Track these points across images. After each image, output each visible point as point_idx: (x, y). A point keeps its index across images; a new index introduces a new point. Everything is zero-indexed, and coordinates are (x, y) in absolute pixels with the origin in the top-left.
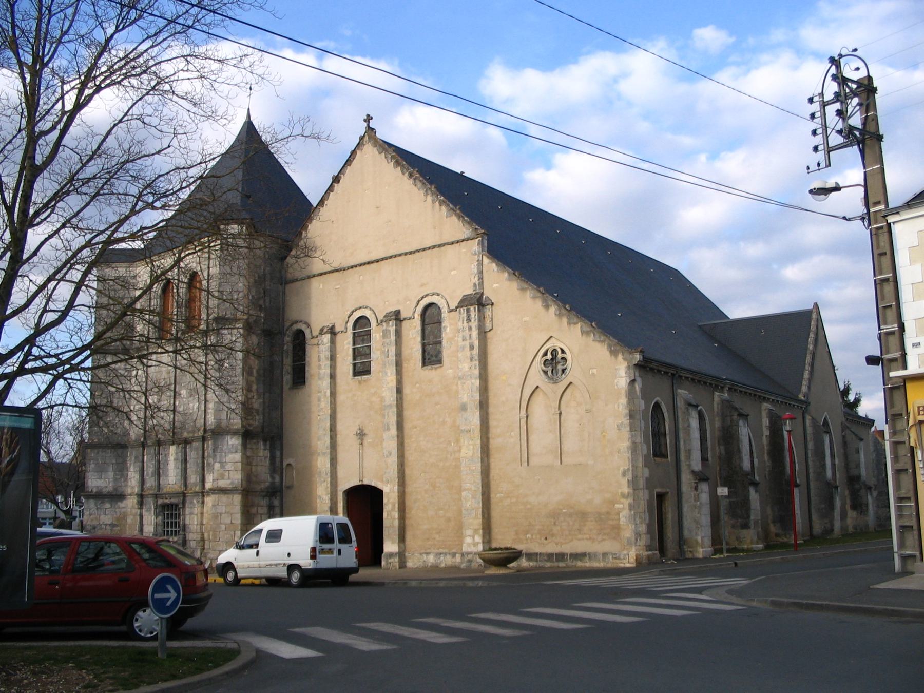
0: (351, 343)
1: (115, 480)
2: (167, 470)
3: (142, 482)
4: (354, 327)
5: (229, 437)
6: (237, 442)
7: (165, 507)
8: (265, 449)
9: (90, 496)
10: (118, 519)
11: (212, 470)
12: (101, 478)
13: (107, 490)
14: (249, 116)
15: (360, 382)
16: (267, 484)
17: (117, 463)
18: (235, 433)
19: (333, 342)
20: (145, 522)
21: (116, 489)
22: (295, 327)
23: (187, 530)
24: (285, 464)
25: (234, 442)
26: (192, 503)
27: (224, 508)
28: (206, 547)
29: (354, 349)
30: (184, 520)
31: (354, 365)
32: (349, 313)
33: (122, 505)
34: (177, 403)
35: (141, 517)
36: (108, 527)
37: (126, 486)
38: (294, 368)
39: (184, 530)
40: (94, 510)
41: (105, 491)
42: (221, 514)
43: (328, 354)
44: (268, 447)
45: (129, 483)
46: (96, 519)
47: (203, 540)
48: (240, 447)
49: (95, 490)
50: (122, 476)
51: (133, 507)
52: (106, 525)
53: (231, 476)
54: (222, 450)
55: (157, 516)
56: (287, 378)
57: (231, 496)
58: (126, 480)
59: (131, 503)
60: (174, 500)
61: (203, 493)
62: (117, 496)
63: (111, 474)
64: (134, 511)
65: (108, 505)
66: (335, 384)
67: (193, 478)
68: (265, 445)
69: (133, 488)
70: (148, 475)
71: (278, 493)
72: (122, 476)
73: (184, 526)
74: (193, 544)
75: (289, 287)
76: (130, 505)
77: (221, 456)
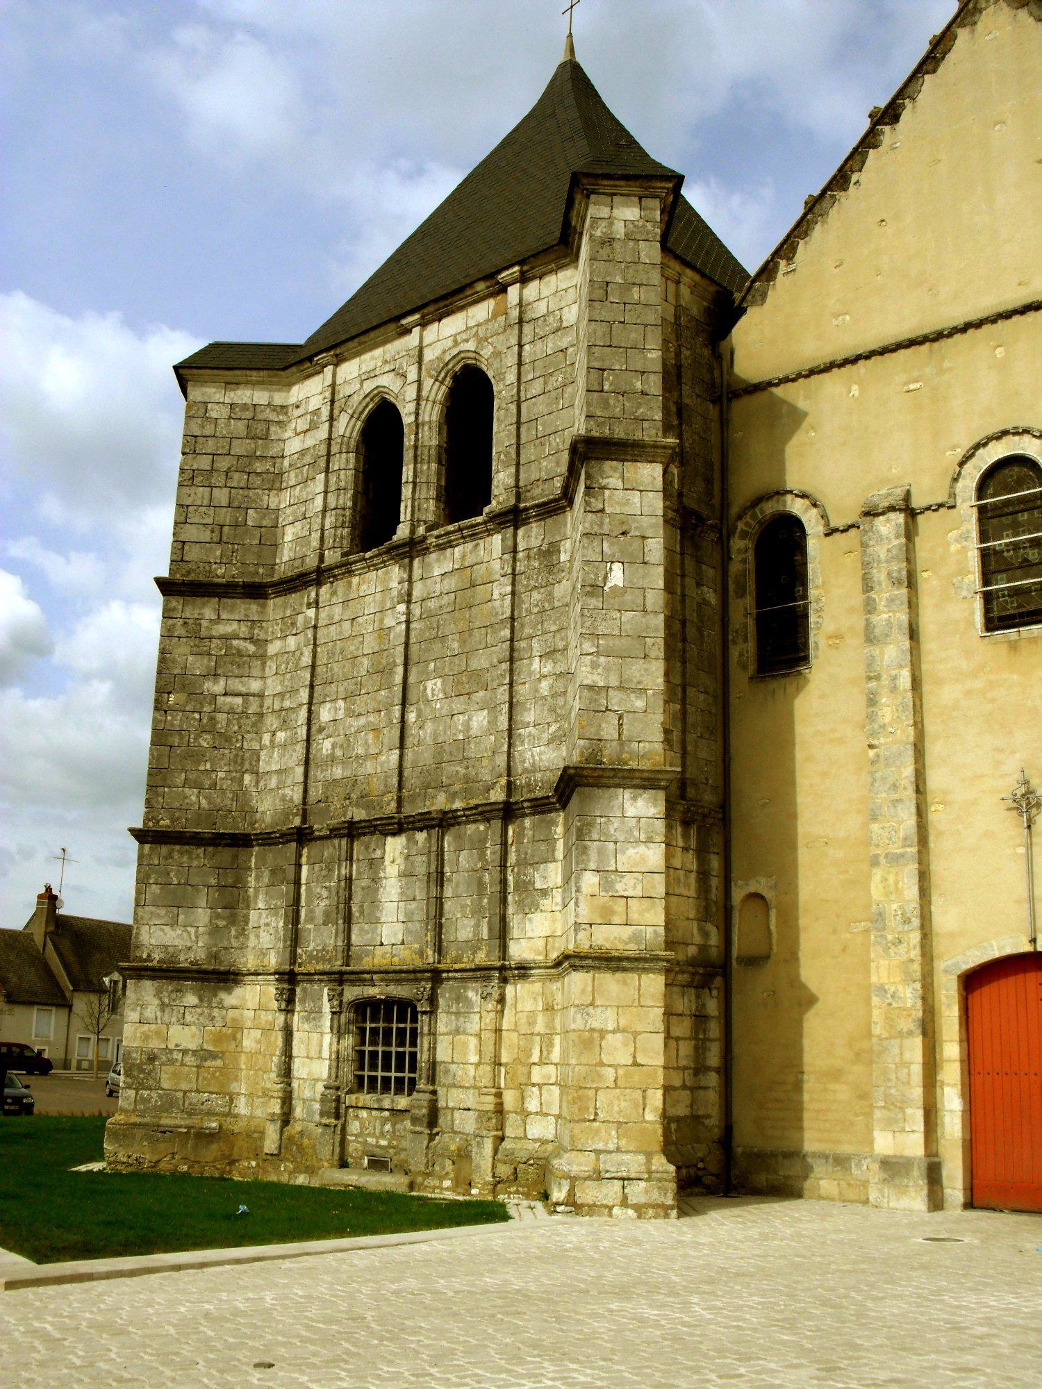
0: (974, 534)
1: (214, 931)
2: (375, 903)
3: (295, 938)
4: (981, 490)
5: (628, 794)
6: (652, 811)
7: (362, 1008)
8: (686, 849)
9: (143, 972)
10: (219, 1039)
11: (531, 897)
12: (173, 924)
13: (192, 956)
14: (572, 50)
15: (1013, 646)
16: (692, 951)
17: (220, 887)
18: (645, 782)
19: (910, 533)
20: (297, 1049)
21: (215, 957)
22: (770, 508)
23: (441, 1078)
24: (738, 895)
25: (641, 810)
26: (459, 998)
27: (611, 1013)
28: (509, 1132)
29: (985, 555)
30: (433, 1049)
31: (988, 598)
32: (960, 453)
33: (230, 999)
34: (412, 717)
35: (288, 1033)
36: (189, 1060)
37: (242, 947)
38: (762, 622)
39: (432, 1079)
40: (152, 1011)
41: (184, 961)
42: (603, 1033)
43: (899, 568)
44: (693, 844)
45: (252, 942)
46: (158, 1033)
47: (500, 1110)
48: (660, 826)
49: (157, 956)
50: (233, 920)
51: (261, 1007)
52: (185, 1052)
53: (634, 916)
54: (606, 837)
55: (339, 1033)
56: (744, 650)
57: (632, 977)
58: (242, 933)
59: (254, 999)
60: (401, 991)
61: (508, 972)
62: (218, 977)
63: (202, 916)
64: (265, 1017)
65: (191, 999)
66: (919, 649)
67: (465, 928)
68: (686, 836)
69: (263, 953)
70: (311, 919)
71: (718, 981)
72: (233, 920)
73: (433, 1065)
74: (466, 1123)
75: (739, 408)
76: (252, 1002)
77: (601, 852)
